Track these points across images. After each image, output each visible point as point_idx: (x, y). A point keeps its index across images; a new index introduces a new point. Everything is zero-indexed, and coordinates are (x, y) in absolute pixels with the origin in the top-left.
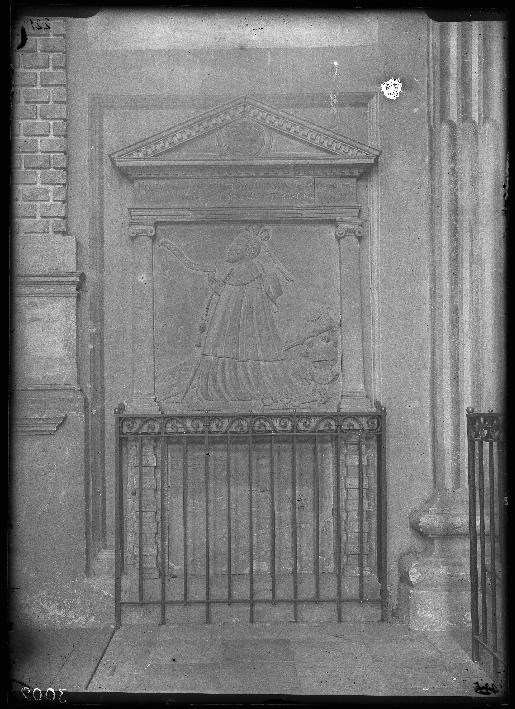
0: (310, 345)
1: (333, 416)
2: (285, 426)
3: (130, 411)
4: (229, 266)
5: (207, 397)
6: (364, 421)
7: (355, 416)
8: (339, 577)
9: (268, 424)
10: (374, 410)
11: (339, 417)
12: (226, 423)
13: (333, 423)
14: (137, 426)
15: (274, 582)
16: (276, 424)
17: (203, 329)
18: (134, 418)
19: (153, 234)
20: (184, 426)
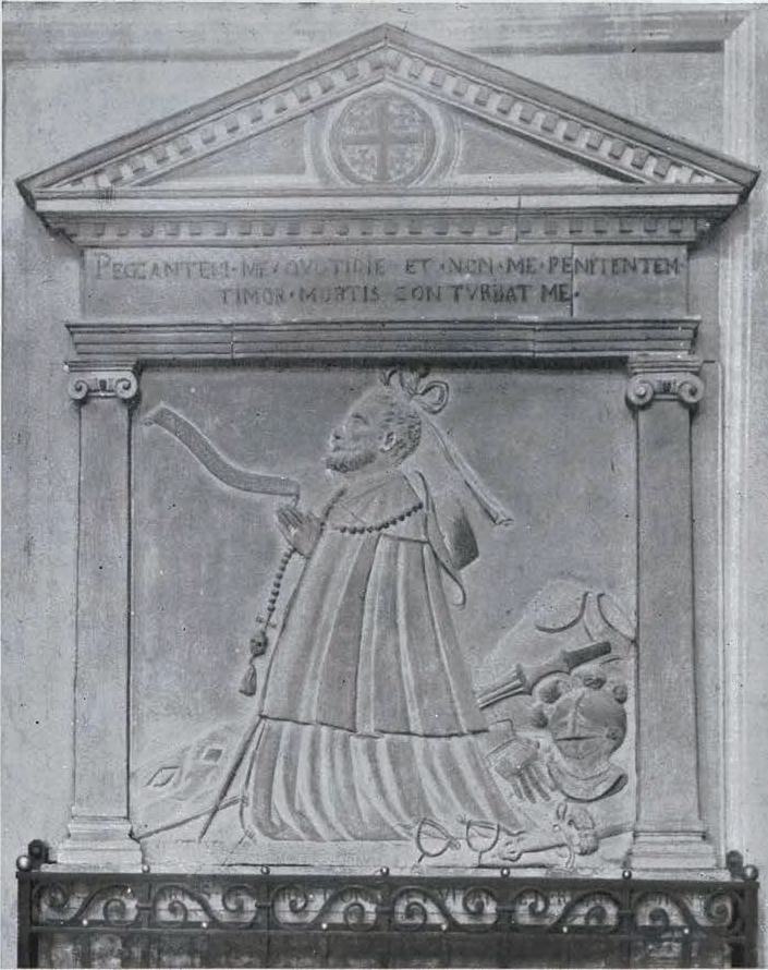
0: (552, 695)
1: (603, 889)
2: (479, 912)
3: (66, 859)
4: (338, 481)
5: (272, 830)
6: (697, 906)
7: (675, 891)
8: (416, 541)
9: (430, 907)
10: (725, 876)
11: (628, 892)
12: (318, 901)
13: (611, 910)
14: (76, 904)
15: (564, 628)
16: (455, 905)
17: (260, 648)
18: (70, 882)
19: (129, 394)
20: (686, 914)
